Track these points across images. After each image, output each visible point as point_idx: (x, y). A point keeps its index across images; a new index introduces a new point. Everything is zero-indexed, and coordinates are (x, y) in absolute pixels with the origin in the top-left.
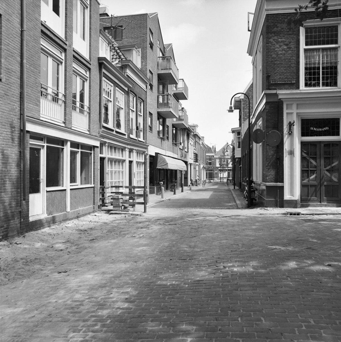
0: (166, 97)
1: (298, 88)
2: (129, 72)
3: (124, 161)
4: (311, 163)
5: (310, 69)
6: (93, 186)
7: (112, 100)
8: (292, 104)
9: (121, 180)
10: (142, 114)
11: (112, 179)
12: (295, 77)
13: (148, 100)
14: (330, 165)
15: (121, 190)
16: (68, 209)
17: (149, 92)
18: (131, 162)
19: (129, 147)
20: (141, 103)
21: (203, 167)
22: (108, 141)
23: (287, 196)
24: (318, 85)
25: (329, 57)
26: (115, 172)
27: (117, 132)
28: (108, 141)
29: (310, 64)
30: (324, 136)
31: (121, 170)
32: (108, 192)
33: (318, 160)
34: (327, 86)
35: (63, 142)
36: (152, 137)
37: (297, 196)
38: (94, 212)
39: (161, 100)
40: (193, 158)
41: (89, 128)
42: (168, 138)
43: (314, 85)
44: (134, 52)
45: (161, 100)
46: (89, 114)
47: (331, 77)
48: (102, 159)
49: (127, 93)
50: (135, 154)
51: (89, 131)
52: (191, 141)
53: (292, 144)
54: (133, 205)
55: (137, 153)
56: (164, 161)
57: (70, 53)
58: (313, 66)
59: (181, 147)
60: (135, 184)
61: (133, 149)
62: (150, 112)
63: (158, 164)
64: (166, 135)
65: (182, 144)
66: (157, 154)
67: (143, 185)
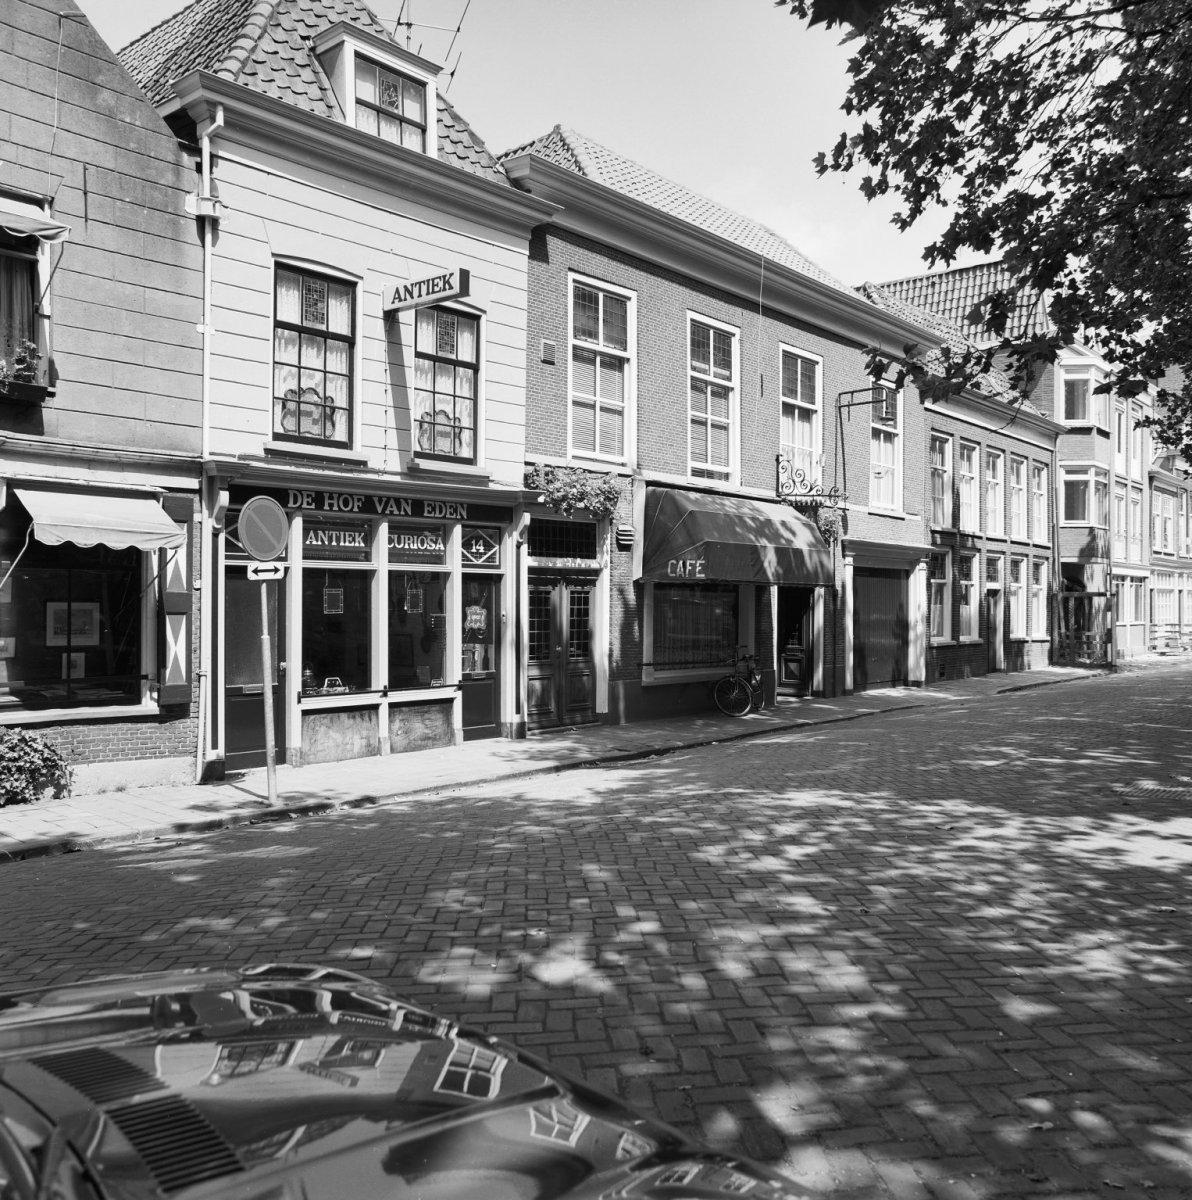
3: (1171, 591)
19: (1179, 571)
32: (1161, 632)
57: (1130, 484)
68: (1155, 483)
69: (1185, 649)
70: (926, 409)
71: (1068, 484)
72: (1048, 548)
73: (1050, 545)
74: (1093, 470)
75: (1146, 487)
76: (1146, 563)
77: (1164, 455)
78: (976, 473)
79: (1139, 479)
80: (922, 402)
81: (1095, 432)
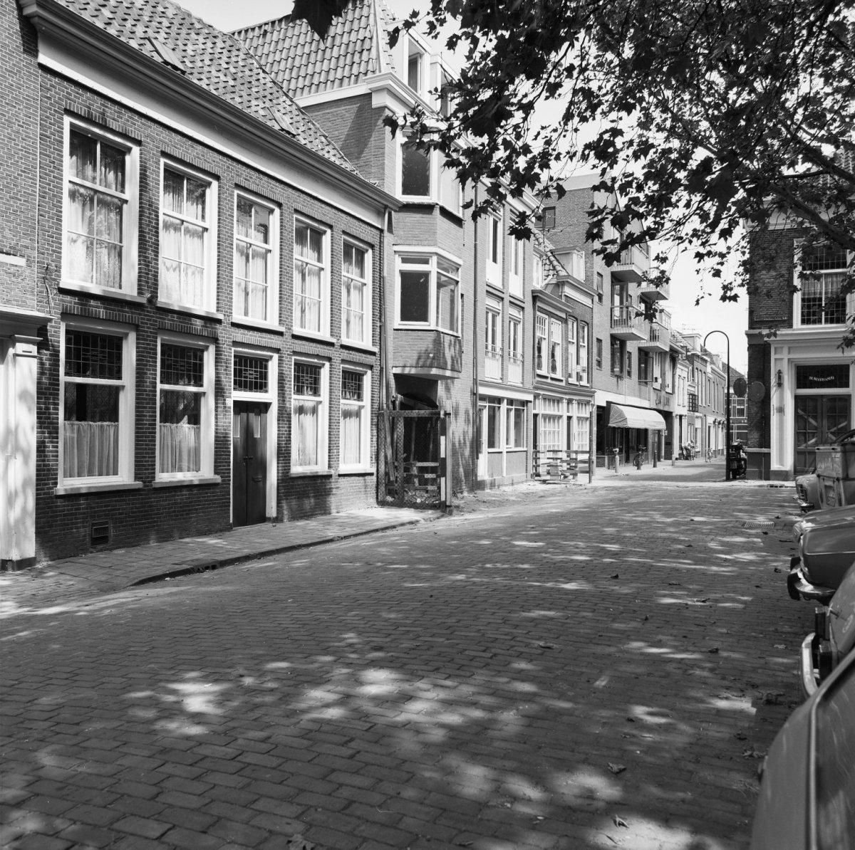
0: (625, 309)
1: (790, 326)
2: (568, 291)
3: (560, 417)
4: (810, 423)
5: (809, 300)
6: (525, 449)
7: (546, 337)
8: (782, 347)
9: (556, 443)
10: (586, 344)
11: (545, 442)
12: (787, 311)
13: (596, 321)
14: (835, 426)
15: (560, 455)
16: (504, 474)
17: (596, 307)
18: (569, 418)
19: (568, 397)
20: (583, 328)
21: (714, 422)
22: (542, 392)
23: (775, 466)
24: (820, 322)
25: (835, 284)
26: (550, 433)
27: (552, 379)
28: (542, 392)
29: (809, 294)
30: (809, 388)
31: (556, 429)
32: (543, 460)
33: (819, 420)
34: (832, 322)
35: (499, 400)
36: (603, 376)
37: (788, 464)
38: (526, 481)
39: (617, 312)
40: (686, 404)
41: (523, 379)
42: (629, 373)
43: (814, 322)
44: (575, 256)
45: (617, 312)
46: (523, 362)
47: (837, 311)
48: (536, 416)
49: (565, 321)
50: (575, 405)
51: (522, 383)
52: (682, 370)
53: (781, 398)
54: (575, 475)
55: (579, 404)
56: (621, 414)
57: (507, 299)
58: (812, 296)
59: (657, 385)
60: (574, 447)
61: (573, 400)
62: (597, 339)
63: (611, 420)
64: (626, 368)
65: (660, 380)
66: (609, 403)
67: (588, 450)
68: (539, 304)
69: (565, 477)
70: (43, 68)
71: (405, 276)
72: (373, 354)
73: (376, 350)
74: (434, 260)
75: (528, 305)
76: (529, 385)
77: (554, 281)
78: (212, 221)
79: (520, 296)
80: (31, 50)
81: (437, 212)
